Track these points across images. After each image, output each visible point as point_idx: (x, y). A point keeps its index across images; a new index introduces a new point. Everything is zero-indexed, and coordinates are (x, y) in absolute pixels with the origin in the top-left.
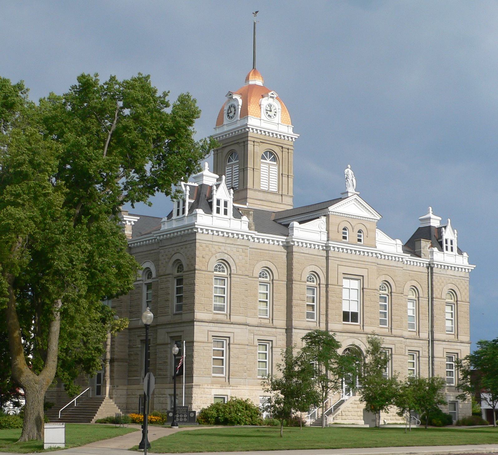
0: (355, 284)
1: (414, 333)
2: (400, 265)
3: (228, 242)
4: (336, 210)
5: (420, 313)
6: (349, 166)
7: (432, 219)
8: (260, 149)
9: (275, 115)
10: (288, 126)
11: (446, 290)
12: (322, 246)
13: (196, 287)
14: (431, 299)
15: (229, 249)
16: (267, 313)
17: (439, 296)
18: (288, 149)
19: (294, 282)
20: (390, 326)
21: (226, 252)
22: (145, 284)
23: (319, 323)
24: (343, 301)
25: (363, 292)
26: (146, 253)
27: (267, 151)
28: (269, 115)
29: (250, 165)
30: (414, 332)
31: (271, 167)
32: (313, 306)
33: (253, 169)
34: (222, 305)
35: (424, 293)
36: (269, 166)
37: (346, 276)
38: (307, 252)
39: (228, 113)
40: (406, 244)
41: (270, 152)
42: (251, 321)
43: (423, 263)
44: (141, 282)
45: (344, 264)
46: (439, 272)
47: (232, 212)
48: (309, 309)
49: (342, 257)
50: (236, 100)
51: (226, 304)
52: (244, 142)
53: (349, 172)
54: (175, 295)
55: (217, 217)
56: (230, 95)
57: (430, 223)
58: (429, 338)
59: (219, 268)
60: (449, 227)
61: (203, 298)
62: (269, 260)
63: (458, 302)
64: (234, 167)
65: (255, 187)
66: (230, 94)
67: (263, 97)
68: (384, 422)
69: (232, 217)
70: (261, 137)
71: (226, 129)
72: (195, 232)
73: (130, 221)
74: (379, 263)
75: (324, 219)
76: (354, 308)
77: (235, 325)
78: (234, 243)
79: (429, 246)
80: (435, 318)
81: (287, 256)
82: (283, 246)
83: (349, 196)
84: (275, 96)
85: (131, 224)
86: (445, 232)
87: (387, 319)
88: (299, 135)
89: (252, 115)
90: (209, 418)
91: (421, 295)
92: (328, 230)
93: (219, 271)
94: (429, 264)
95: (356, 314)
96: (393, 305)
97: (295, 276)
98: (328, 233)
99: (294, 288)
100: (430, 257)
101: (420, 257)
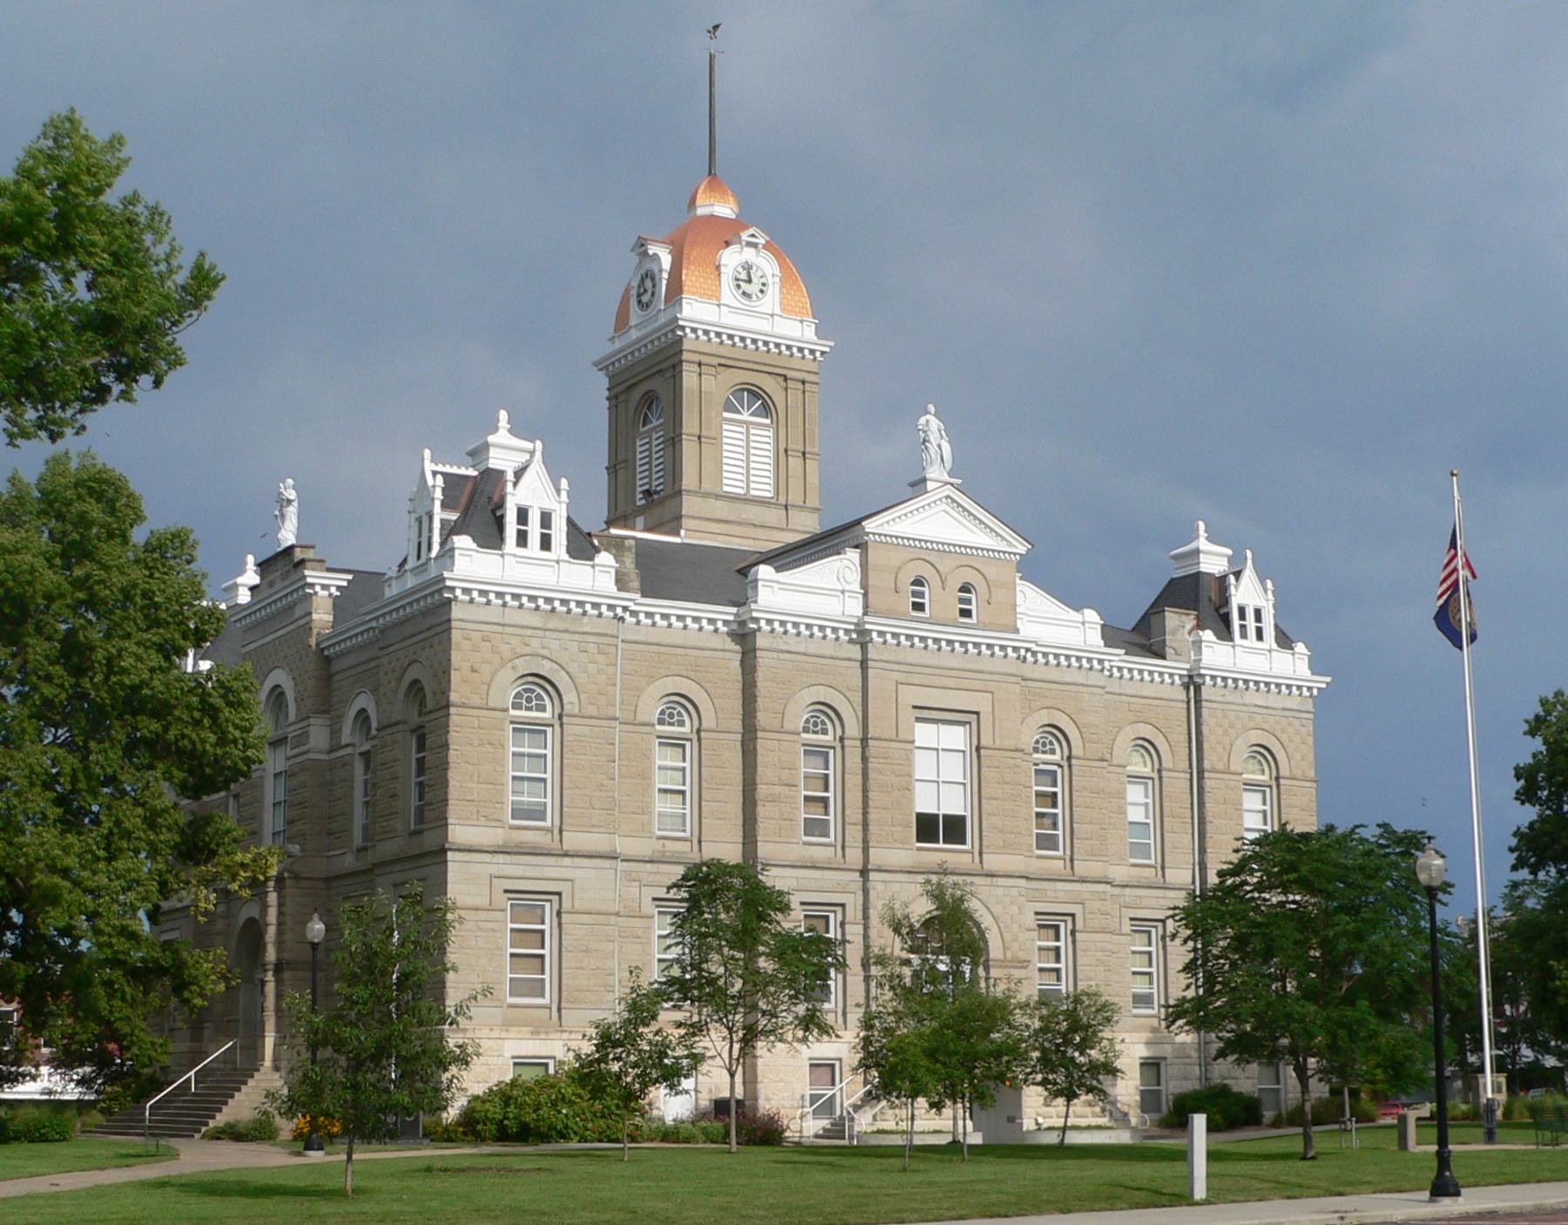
0: (956, 737)
1: (1147, 870)
2: (1095, 679)
3: (552, 624)
4: (886, 530)
5: (1165, 814)
6: (931, 408)
7: (1204, 552)
8: (717, 385)
9: (762, 291)
10: (802, 322)
11: (1241, 749)
12: (847, 631)
13: (452, 753)
14: (1198, 773)
15: (555, 645)
16: (684, 825)
17: (1221, 766)
18: (803, 382)
19: (759, 734)
20: (1068, 852)
21: (545, 652)
22: (360, 754)
23: (843, 848)
24: (917, 784)
25: (979, 757)
26: (360, 669)
27: (743, 390)
28: (744, 293)
29: (689, 425)
30: (685, 840)
31: (752, 431)
32: (825, 801)
33: (699, 438)
34: (538, 804)
35: (1175, 757)
36: (748, 431)
37: (926, 714)
38: (802, 649)
39: (639, 296)
40: (1137, 625)
41: (749, 391)
42: (623, 845)
43: (1171, 675)
44: (349, 750)
45: (916, 679)
46: (1221, 699)
47: (565, 542)
48: (812, 810)
49: (910, 660)
50: (656, 257)
51: (549, 800)
52: (674, 367)
53: (931, 423)
54: (414, 780)
55: (515, 556)
56: (643, 245)
57: (1198, 563)
58: (1194, 882)
59: (529, 700)
60: (1249, 573)
61: (474, 785)
62: (685, 673)
63: (1282, 781)
64: (655, 436)
65: (706, 487)
66: (641, 244)
67: (727, 244)
68: (1037, 1124)
69: (1275, 646)
70: (722, 351)
71: (634, 335)
72: (449, 601)
73: (325, 587)
74: (1029, 675)
75: (853, 555)
76: (952, 803)
77: (576, 860)
78: (573, 628)
79: (1189, 627)
80: (1209, 828)
81: (742, 662)
82: (731, 634)
83: (929, 489)
84: (761, 241)
85: (330, 595)
86: (1236, 587)
87: (1060, 832)
88: (832, 344)
89: (693, 294)
90: (478, 1123)
91: (1167, 763)
92: (864, 585)
93: (528, 709)
94: (1191, 677)
95: (962, 819)
96: (1075, 794)
97: (762, 718)
98: (865, 595)
99: (760, 750)
100: (1193, 658)
101: (1163, 657)
